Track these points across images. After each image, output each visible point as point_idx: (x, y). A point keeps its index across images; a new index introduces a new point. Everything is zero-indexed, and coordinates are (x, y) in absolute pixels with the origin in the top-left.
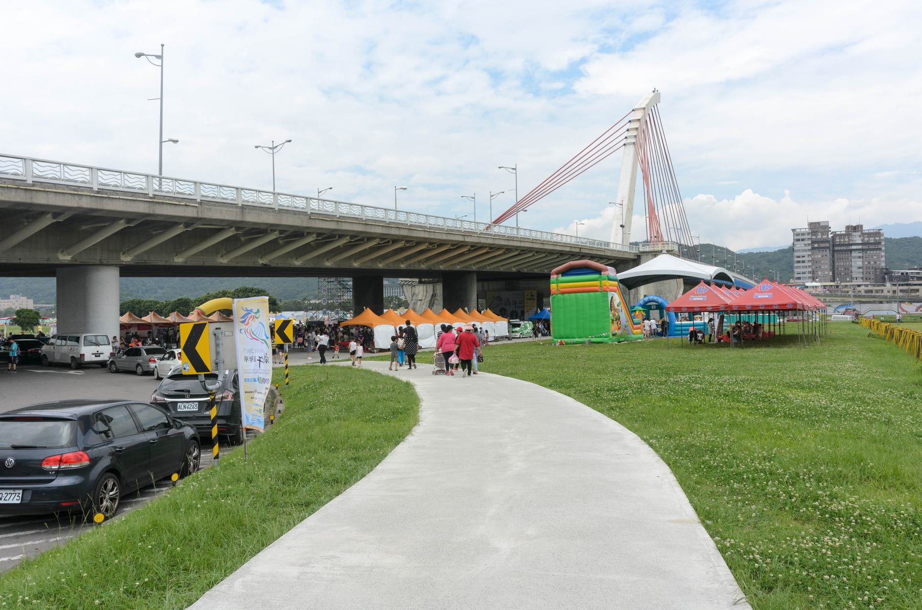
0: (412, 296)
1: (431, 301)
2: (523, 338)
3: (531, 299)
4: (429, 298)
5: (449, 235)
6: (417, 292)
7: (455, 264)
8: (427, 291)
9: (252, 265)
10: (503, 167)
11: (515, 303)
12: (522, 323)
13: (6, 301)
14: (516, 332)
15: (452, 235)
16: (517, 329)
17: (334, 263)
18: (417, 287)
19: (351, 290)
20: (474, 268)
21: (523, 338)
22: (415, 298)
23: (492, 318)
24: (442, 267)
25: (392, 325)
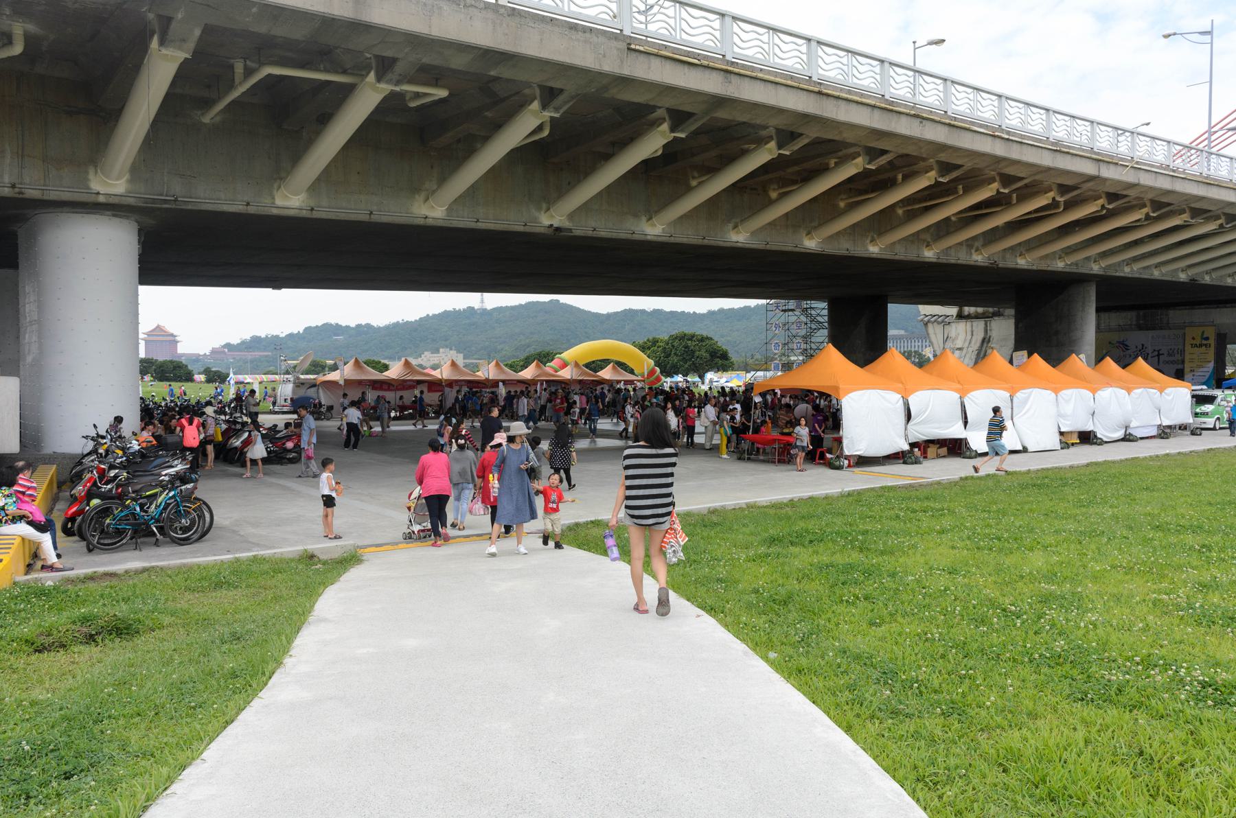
0: (945, 341)
1: (979, 350)
2: (1220, 428)
3: (1201, 345)
4: (976, 345)
5: (1059, 156)
6: (953, 334)
7: (1052, 256)
8: (972, 332)
9: (521, 229)
10: (1175, 34)
11: (1159, 355)
12: (1218, 393)
13: (436, 355)
14: (1205, 414)
15: (1069, 157)
16: (1208, 408)
17: (753, 233)
18: (953, 325)
19: (826, 324)
20: (1096, 268)
21: (1220, 428)
22: (949, 344)
23: (1154, 380)
24: (1022, 262)
25: (956, 390)
